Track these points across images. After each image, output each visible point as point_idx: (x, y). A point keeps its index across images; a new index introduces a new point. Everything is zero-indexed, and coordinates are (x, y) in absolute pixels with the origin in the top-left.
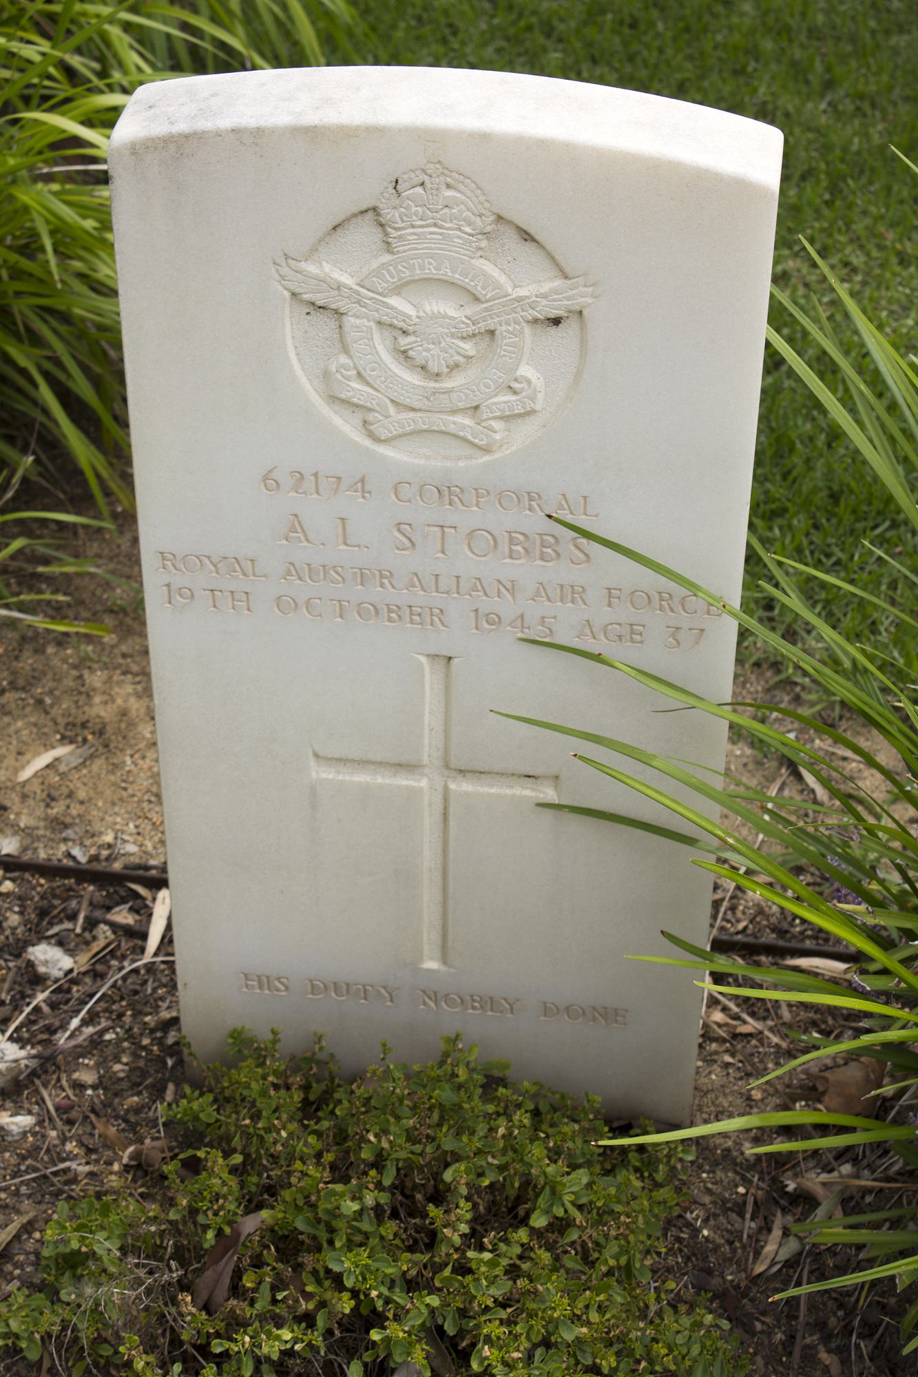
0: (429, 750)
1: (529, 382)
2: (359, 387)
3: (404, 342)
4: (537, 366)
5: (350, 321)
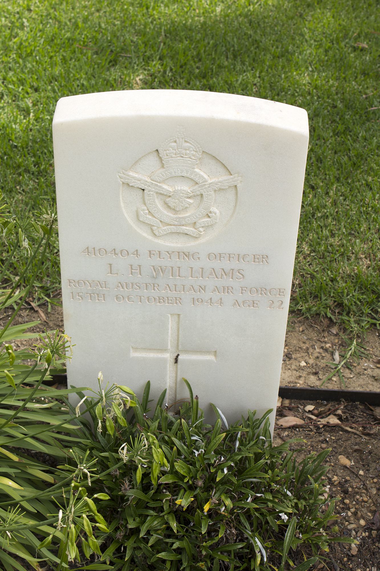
2: (150, 217)
3: (168, 200)
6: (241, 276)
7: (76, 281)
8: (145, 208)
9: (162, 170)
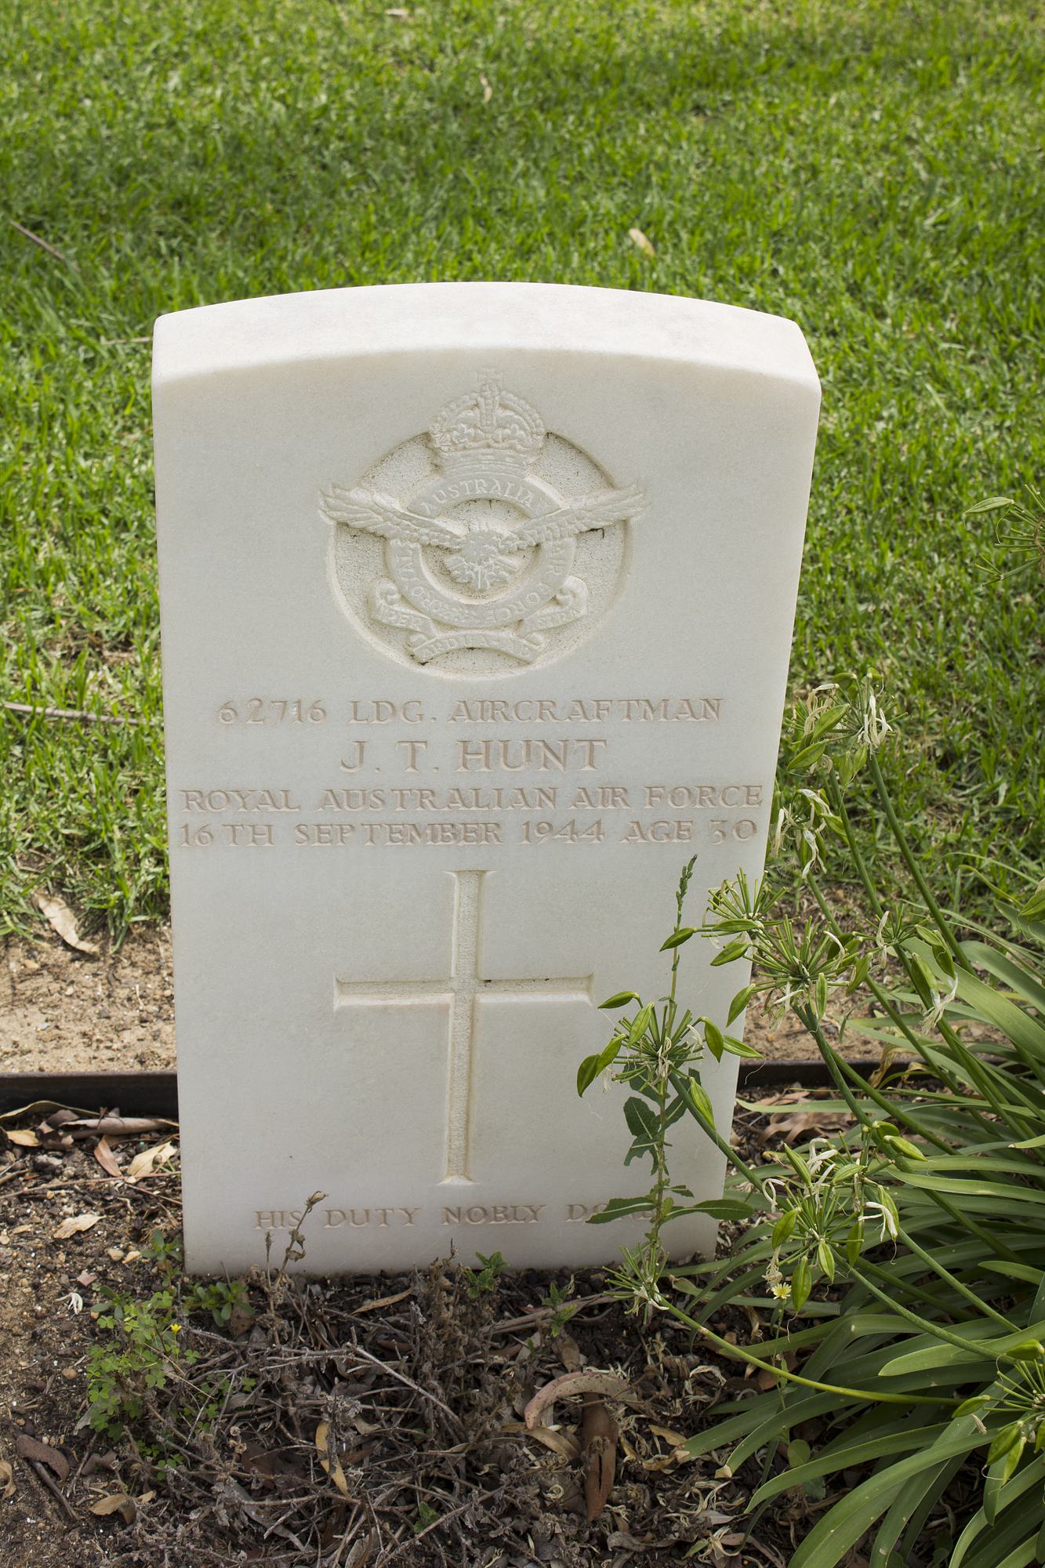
0: (457, 963)
3: (449, 560)
7: (205, 793)
8: (393, 587)
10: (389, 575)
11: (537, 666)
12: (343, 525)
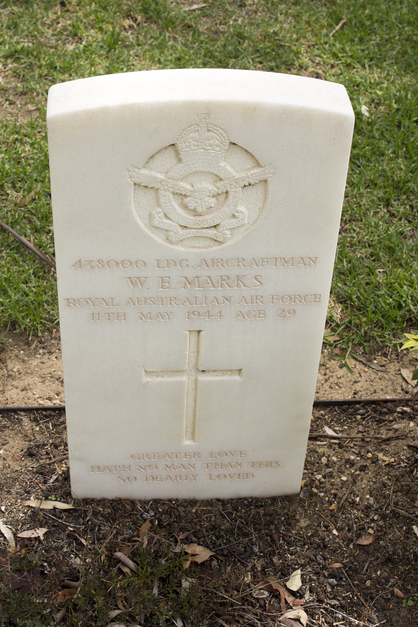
1: (242, 212)
4: (245, 206)
5: (162, 192)
6: (258, 283)
9: (180, 165)
10: (159, 205)
11: (226, 245)
12: (135, 184)
